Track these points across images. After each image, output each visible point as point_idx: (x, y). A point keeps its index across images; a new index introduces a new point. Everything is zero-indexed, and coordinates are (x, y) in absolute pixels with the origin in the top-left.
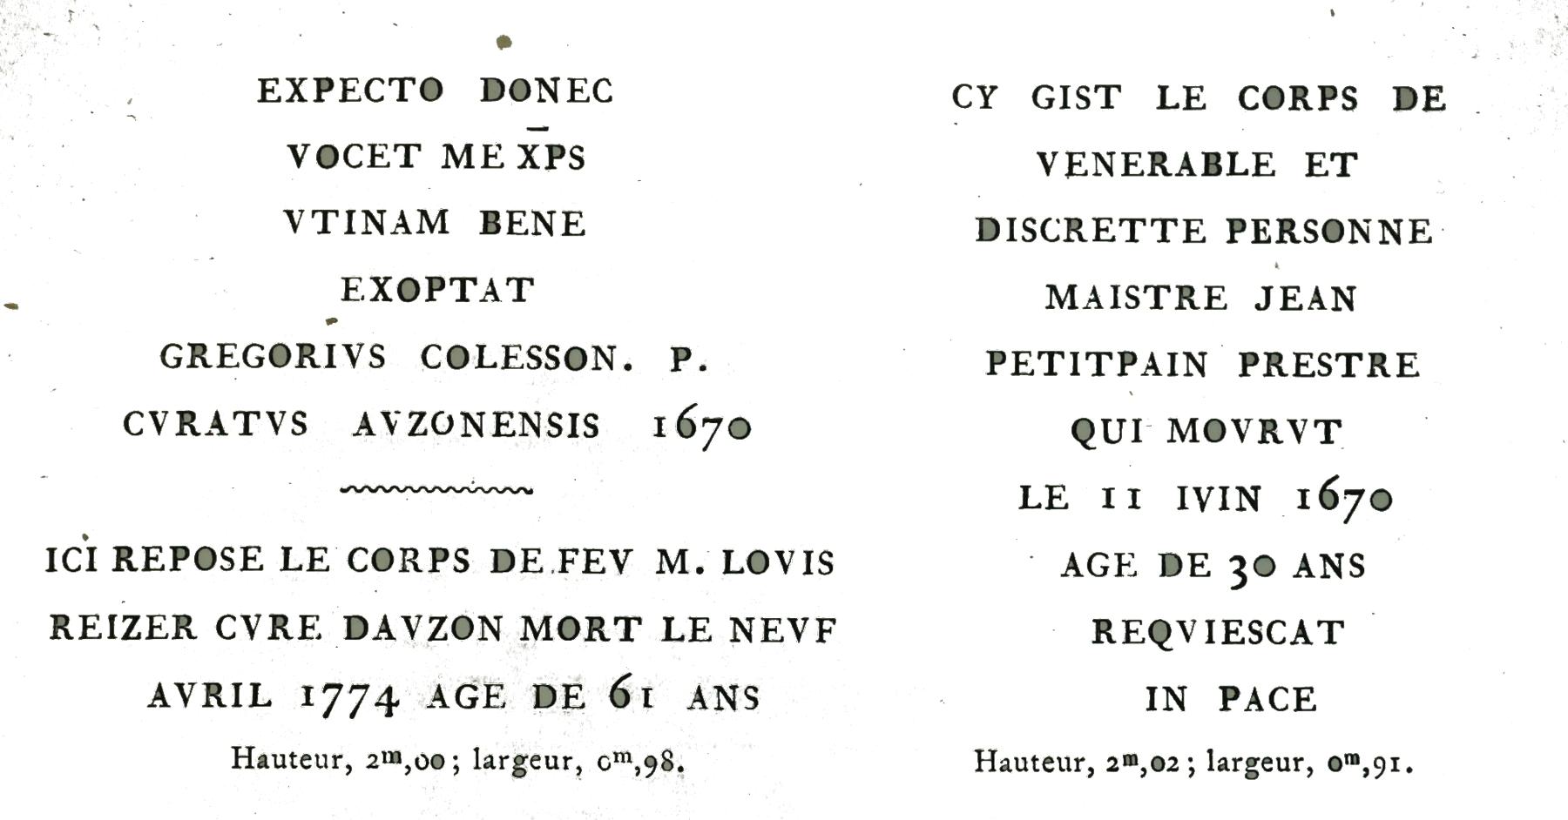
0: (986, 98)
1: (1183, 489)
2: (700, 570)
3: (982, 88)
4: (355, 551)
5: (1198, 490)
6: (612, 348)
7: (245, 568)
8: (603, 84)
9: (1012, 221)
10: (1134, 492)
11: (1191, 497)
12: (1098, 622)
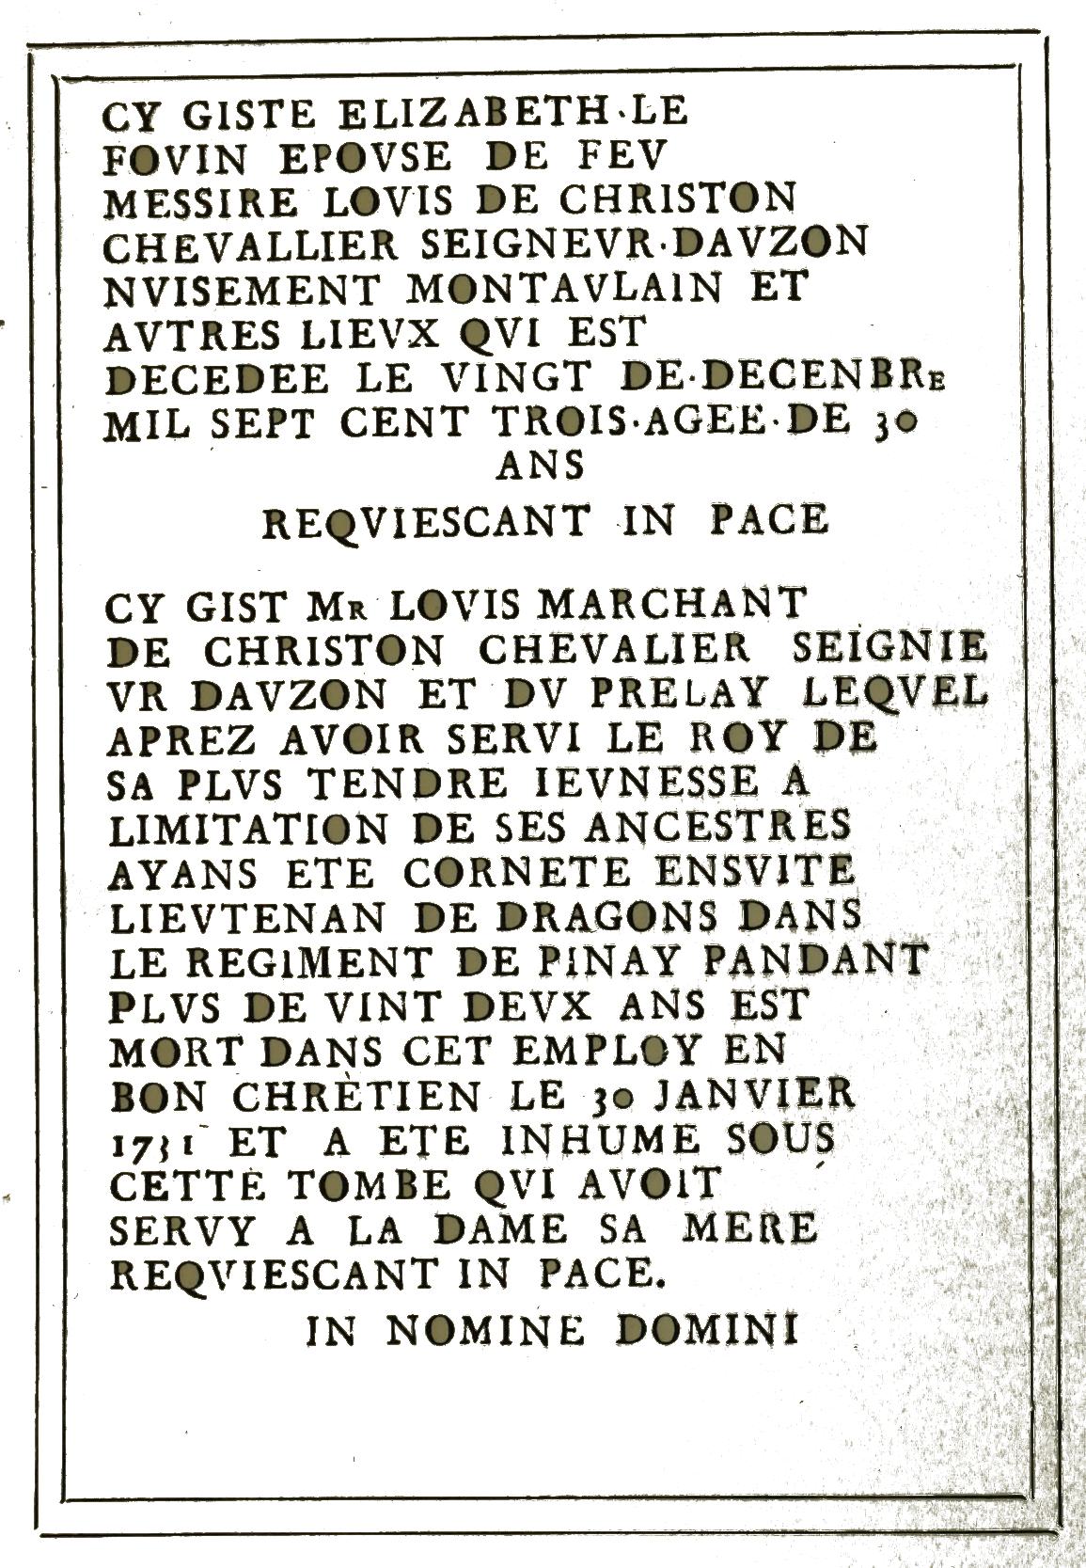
0: (150, 611)
3: (143, 597)
12: (269, 513)
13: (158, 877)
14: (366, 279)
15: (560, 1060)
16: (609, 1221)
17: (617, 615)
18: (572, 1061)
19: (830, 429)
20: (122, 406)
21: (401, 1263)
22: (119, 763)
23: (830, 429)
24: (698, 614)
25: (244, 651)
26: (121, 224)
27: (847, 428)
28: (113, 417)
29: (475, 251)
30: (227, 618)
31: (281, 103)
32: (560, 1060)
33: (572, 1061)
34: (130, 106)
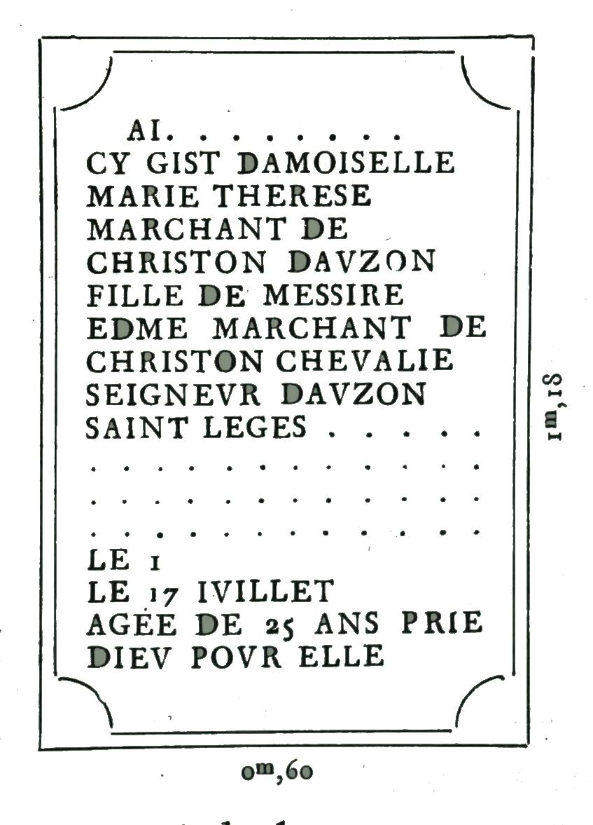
0: (120, 165)
1: (202, 584)
2: (170, 138)
3: (115, 155)
4: (222, 253)
5: (215, 584)
6: (431, 251)
7: (374, 170)
8: (287, 635)
9: (344, 154)
10: (155, 558)
11: (209, 589)
13: (123, 165)
14: (276, 221)
15: (225, 335)
16: (93, 422)
17: (270, 337)
18: (285, 303)
19: (471, 334)
20: (101, 214)
21: (258, 219)
22: (92, 412)
23: (471, 334)
24: (331, 336)
25: (116, 361)
26: (100, 244)
27: (484, 334)
28: (94, 189)
29: (127, 400)
30: (176, 171)
31: (231, 187)
32: (225, 335)
33: (285, 303)
34: (107, 155)
